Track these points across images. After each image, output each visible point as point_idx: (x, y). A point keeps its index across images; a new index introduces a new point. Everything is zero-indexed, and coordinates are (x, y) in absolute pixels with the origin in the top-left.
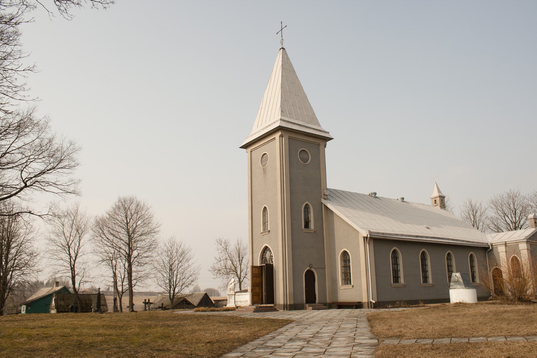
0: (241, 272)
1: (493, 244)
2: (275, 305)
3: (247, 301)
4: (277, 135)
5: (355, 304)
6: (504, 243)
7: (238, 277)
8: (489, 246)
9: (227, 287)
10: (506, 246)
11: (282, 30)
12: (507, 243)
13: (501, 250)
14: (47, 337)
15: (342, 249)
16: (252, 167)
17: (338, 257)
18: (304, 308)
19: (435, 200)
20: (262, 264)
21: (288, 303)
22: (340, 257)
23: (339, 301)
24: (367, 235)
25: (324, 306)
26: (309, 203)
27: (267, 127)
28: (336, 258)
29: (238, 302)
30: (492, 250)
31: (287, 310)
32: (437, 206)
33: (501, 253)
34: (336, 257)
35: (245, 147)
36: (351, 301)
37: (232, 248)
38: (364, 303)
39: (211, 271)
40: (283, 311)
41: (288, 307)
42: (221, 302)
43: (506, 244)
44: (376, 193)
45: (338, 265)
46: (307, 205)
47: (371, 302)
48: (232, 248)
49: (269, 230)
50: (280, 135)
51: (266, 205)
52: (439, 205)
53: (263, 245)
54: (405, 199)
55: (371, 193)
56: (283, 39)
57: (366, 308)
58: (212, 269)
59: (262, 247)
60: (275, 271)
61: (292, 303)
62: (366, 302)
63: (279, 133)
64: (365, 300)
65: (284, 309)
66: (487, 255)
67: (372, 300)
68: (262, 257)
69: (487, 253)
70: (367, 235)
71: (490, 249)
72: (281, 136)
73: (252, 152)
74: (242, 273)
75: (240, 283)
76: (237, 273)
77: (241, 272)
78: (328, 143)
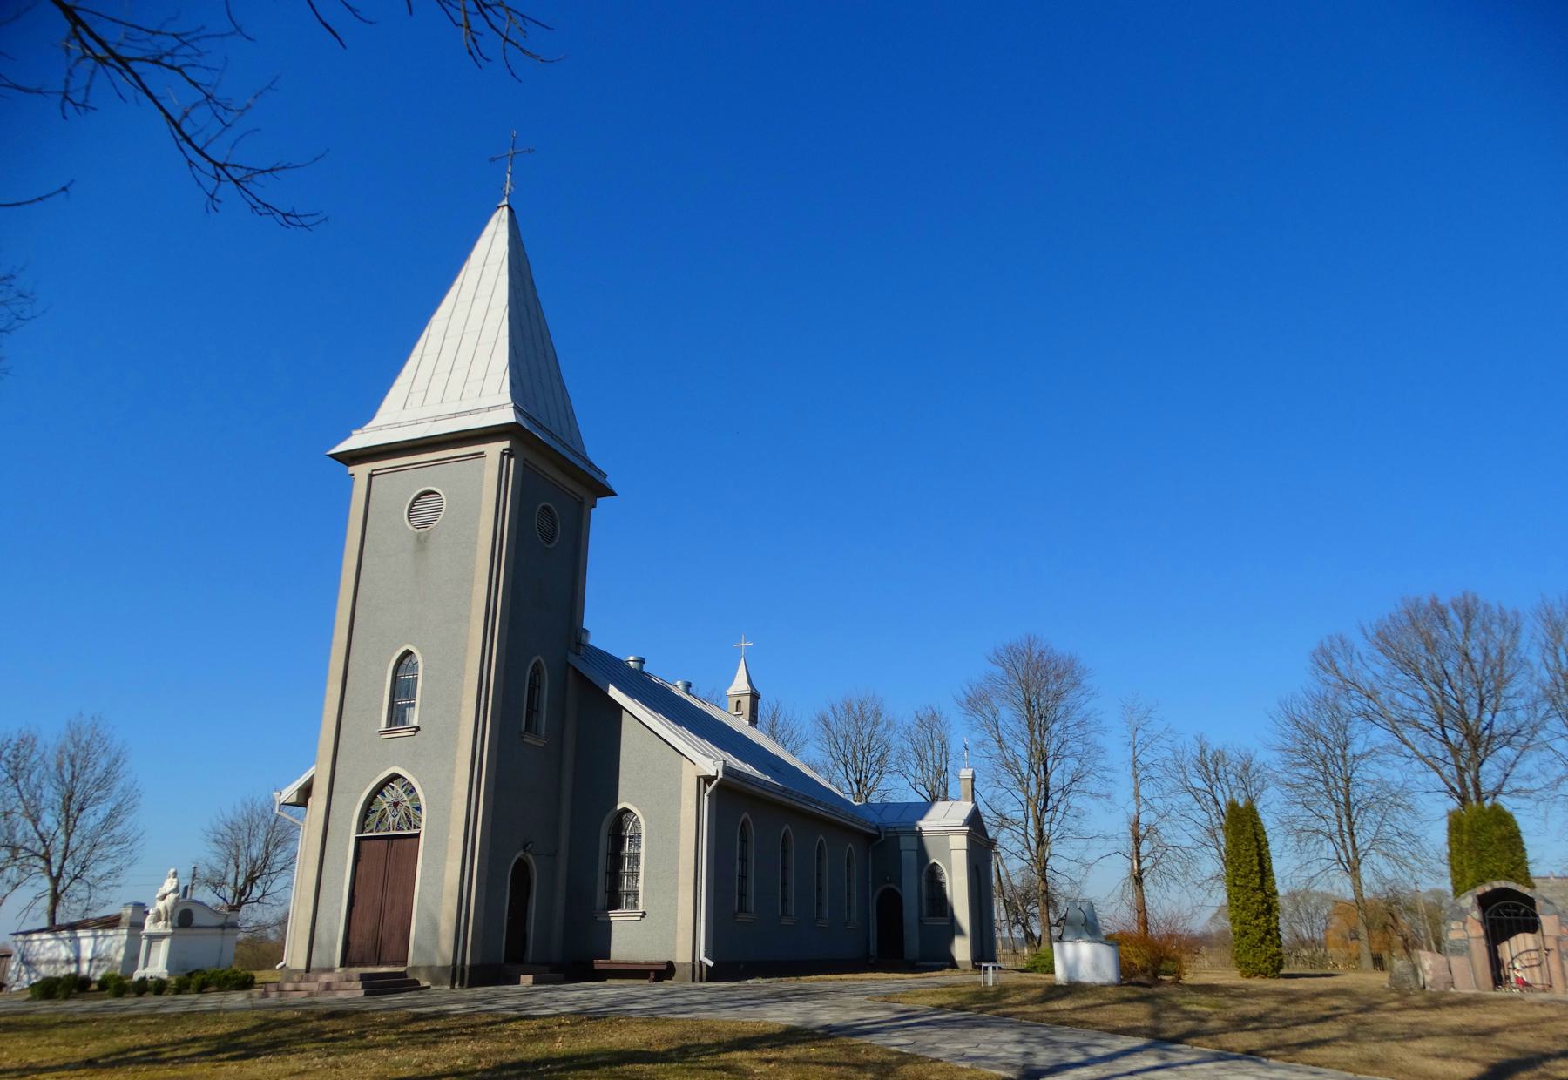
4: (494, 450)
8: (880, 832)
14: (1099, 1030)
20: (362, 833)
24: (717, 772)
26: (542, 661)
27: (456, 415)
32: (740, 717)
33: (906, 852)
38: (679, 964)
41: (467, 975)
49: (415, 722)
50: (504, 450)
51: (411, 643)
53: (381, 771)
63: (506, 444)
64: (682, 956)
67: (705, 956)
68: (369, 809)
70: (717, 772)
71: (880, 841)
75: (55, 898)
76: (48, 862)
78: (602, 502)
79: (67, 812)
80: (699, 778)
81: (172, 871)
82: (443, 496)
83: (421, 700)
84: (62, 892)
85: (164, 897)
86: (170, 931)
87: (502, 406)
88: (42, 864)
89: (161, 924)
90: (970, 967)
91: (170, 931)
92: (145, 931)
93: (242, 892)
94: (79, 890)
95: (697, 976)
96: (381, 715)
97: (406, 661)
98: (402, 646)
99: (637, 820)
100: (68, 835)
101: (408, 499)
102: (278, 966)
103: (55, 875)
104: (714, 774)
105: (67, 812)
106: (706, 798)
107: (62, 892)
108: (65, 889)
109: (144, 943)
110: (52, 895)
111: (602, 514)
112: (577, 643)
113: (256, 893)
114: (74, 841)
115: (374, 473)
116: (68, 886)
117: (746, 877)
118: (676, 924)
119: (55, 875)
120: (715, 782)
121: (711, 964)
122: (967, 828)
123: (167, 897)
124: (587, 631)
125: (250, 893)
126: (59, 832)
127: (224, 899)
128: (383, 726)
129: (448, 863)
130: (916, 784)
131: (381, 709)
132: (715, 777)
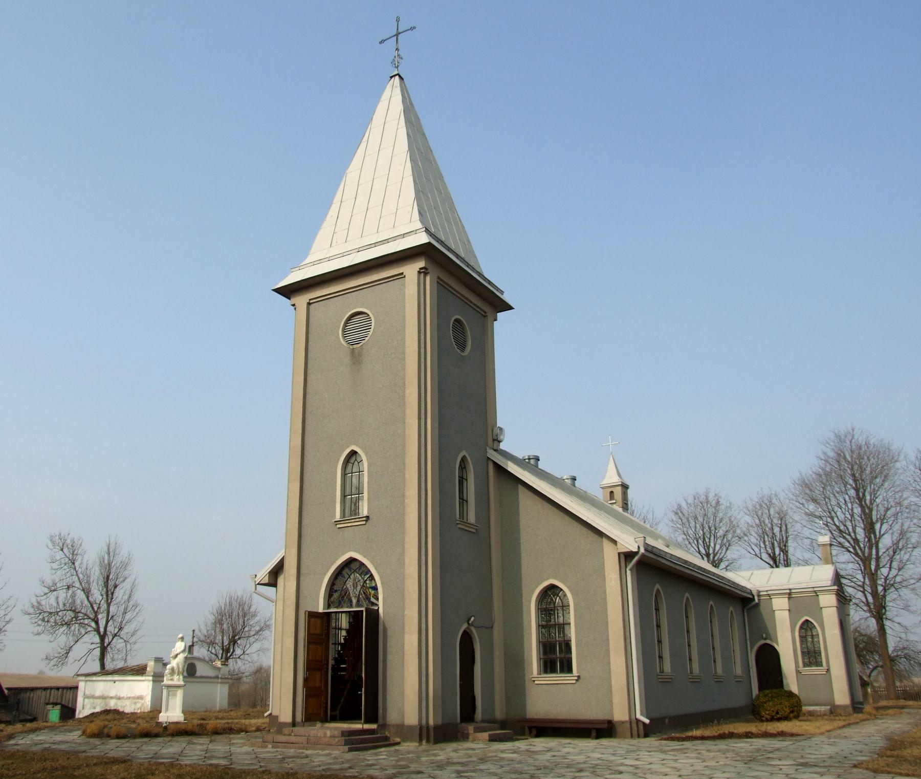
0: (107, 622)
1: (762, 593)
2: (384, 726)
3: (141, 698)
4: (411, 270)
5: (536, 725)
6: (788, 591)
7: (99, 632)
8: (753, 596)
9: (66, 657)
10: (789, 598)
11: (397, 35)
12: (793, 591)
13: (780, 605)
15: (542, 581)
16: (310, 343)
17: (530, 602)
18: (459, 735)
19: (612, 492)
21: (431, 722)
22: (536, 600)
23: (528, 717)
24: (639, 547)
25: (502, 729)
26: (467, 456)
27: (376, 244)
28: (522, 602)
29: (112, 698)
30: (757, 605)
31: (428, 741)
34: (524, 600)
35: (288, 292)
36: (568, 718)
37: (91, 558)
38: (617, 722)
39: (30, 614)
40: (417, 744)
42: (28, 694)
43: (790, 595)
44: (538, 457)
45: (530, 622)
46: (464, 456)
47: (638, 721)
48: (91, 558)
49: (365, 513)
50: (420, 269)
52: (621, 503)
53: (340, 556)
54: (577, 479)
55: (529, 456)
56: (402, 55)
57: (625, 737)
58: (31, 610)
59: (336, 560)
60: (385, 629)
61: (440, 722)
62: (626, 721)
63: (421, 264)
64: (620, 714)
65: (421, 740)
66: (746, 614)
69: (745, 610)
71: (754, 603)
72: (423, 272)
73: (313, 305)
74: (110, 623)
75: (104, 650)
76: (97, 623)
77: (107, 622)
79: (107, 587)
80: (619, 554)
81: (180, 636)
82: (371, 316)
83: (369, 493)
84: (108, 645)
85: (176, 656)
86: (182, 683)
87: (415, 232)
88: (93, 624)
89: (176, 677)
90: (850, 710)
91: (182, 683)
92: (164, 683)
93: (228, 650)
94: (118, 643)
95: (635, 733)
96: (335, 508)
97: (352, 460)
98: (348, 447)
99: (565, 595)
100: (109, 605)
101: (341, 320)
102: (266, 714)
103: (102, 633)
104: (636, 550)
105: (107, 587)
106: (629, 572)
107: (108, 645)
108: (109, 644)
109: (165, 691)
110: (101, 647)
111: (502, 323)
112: (494, 440)
113: (238, 651)
114: (113, 609)
115: (311, 302)
116: (111, 641)
117: (661, 642)
118: (611, 686)
119: (102, 633)
120: (636, 558)
121: (647, 721)
122: (836, 587)
123: (178, 656)
124: (501, 429)
125: (234, 651)
126: (103, 601)
127: (216, 655)
128: (338, 516)
129: (407, 636)
130: (761, 553)
131: (335, 502)
132: (636, 553)
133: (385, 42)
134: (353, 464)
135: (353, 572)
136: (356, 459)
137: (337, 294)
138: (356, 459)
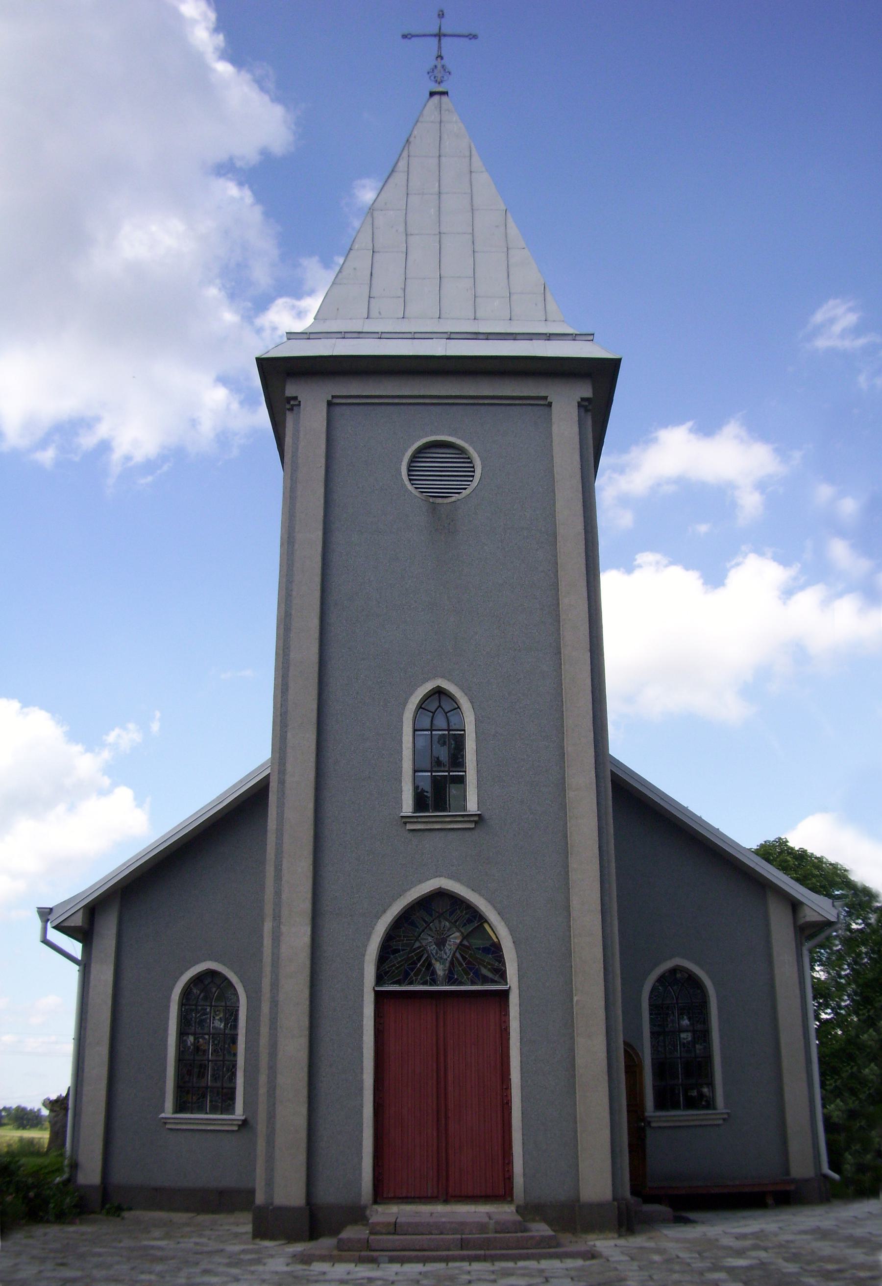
38: (48, 1109)
47: (825, 1177)
50: (583, 399)
53: (413, 885)
133: (413, 39)
134: (434, 713)
135: (438, 917)
136: (440, 706)
137: (396, 401)
138: (440, 706)
